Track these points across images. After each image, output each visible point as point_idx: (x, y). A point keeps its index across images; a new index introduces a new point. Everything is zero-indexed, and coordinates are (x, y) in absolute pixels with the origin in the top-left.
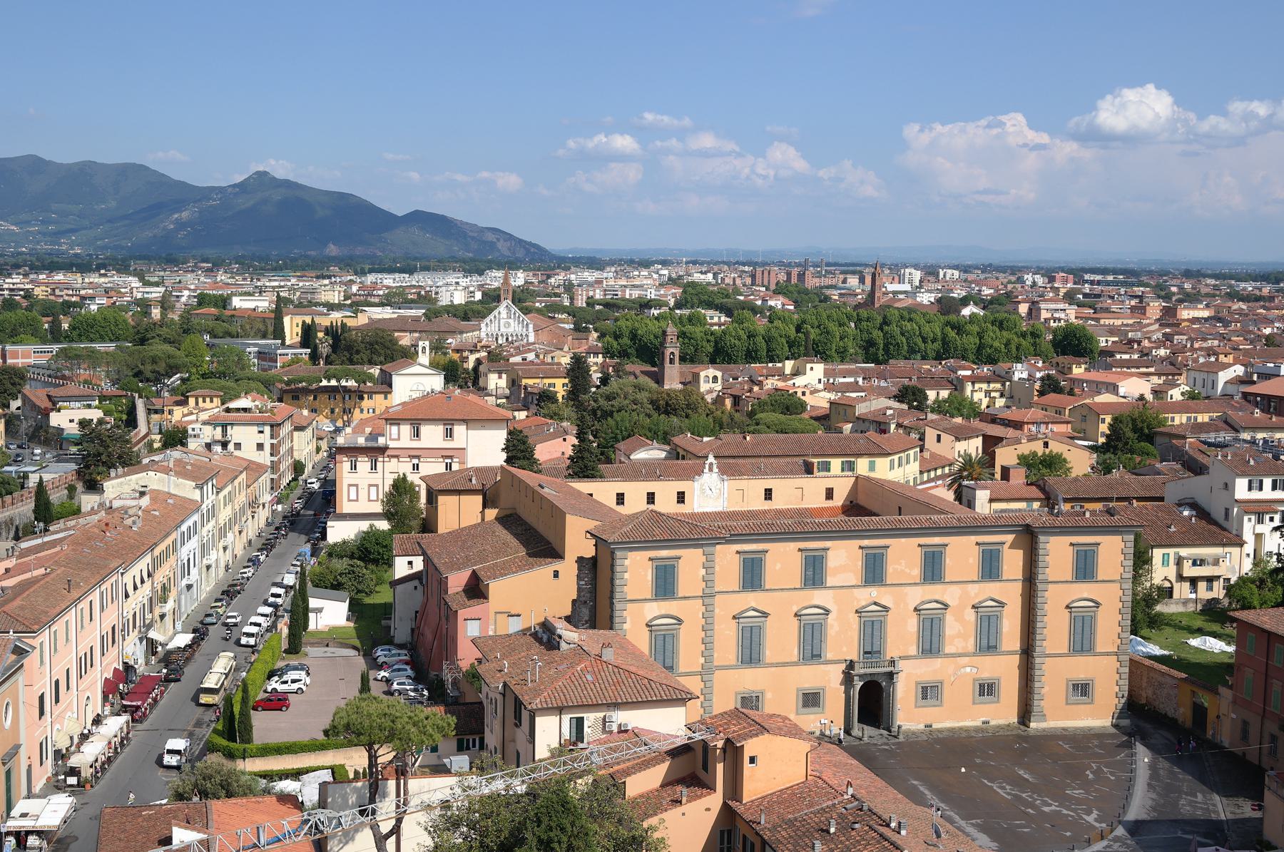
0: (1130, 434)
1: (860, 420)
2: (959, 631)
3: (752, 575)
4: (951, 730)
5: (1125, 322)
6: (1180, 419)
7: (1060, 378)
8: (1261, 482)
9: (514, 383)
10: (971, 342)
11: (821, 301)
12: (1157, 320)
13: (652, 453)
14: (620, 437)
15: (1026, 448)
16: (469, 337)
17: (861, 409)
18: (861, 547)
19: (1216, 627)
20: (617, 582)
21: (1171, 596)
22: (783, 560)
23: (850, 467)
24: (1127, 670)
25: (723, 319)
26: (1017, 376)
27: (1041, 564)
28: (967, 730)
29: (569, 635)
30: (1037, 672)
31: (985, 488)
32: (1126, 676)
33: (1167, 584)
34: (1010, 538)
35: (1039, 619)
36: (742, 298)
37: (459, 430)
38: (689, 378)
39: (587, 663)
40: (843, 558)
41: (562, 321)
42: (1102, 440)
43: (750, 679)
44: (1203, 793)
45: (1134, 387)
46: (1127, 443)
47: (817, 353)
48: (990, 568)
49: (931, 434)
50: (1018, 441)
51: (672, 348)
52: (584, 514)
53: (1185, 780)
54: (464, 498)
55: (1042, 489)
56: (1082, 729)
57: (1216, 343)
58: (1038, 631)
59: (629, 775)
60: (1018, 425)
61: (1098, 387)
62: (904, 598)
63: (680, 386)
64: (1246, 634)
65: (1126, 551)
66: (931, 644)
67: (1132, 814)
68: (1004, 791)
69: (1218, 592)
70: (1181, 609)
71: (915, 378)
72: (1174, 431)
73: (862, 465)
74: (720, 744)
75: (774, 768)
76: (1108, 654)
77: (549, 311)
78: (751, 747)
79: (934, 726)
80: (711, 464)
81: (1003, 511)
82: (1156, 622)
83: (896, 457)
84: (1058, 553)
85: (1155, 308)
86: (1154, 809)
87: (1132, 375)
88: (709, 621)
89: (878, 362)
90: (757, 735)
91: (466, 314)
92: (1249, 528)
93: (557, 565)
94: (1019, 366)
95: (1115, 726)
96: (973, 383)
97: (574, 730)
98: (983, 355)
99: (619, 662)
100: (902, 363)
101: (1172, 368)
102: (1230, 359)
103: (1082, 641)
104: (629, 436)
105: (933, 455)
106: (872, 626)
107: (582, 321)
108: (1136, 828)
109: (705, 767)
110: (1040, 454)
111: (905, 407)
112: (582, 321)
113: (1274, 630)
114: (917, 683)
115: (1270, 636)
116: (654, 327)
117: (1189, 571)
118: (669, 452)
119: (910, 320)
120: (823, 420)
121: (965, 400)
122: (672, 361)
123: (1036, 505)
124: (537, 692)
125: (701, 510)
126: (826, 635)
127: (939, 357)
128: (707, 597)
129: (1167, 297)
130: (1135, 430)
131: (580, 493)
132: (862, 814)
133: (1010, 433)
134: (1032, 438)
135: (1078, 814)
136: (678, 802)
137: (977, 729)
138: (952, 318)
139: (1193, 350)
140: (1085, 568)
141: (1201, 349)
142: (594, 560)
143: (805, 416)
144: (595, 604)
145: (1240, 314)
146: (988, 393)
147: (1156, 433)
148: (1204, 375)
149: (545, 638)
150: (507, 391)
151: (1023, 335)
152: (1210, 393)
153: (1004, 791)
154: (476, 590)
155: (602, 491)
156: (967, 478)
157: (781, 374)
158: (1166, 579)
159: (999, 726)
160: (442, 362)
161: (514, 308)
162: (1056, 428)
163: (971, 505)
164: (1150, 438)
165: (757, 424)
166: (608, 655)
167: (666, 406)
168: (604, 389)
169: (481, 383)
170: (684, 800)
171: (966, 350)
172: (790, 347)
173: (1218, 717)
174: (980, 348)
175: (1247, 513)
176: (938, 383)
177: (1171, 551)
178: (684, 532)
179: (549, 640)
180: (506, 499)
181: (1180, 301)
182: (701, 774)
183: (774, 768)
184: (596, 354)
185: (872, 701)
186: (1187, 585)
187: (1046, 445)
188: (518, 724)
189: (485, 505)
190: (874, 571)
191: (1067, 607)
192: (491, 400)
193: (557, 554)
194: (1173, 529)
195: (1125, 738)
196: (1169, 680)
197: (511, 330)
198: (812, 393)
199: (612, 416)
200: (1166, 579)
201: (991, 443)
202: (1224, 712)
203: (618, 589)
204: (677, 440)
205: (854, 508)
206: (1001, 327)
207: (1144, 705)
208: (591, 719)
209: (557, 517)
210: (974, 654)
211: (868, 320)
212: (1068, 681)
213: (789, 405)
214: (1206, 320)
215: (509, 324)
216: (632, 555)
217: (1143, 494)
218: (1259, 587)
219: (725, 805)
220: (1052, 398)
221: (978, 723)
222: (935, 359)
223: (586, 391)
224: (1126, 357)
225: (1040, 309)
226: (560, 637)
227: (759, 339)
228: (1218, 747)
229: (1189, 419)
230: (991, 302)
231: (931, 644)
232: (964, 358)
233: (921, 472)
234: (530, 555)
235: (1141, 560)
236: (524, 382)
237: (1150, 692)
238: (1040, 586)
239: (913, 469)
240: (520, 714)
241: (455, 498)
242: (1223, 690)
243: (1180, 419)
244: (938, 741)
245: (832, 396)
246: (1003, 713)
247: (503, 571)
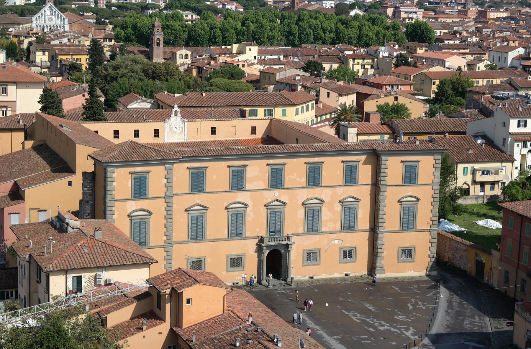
0: (450, 92)
1: (279, 82)
2: (331, 218)
3: (198, 183)
4: (326, 280)
5: (454, 20)
6: (482, 82)
7: (408, 55)
8: (526, 121)
9: (53, 58)
10: (354, 32)
11: (261, 6)
12: (474, 19)
13: (141, 104)
14: (122, 94)
15: (382, 101)
16: (24, 27)
17: (280, 76)
18: (268, 165)
19: (495, 213)
20: (108, 188)
21: (468, 194)
22: (218, 173)
23: (270, 113)
24: (436, 240)
25: (195, 16)
26: (382, 54)
27: (382, 174)
28: (335, 279)
29: (74, 223)
30: (380, 243)
31: (354, 126)
32: (435, 244)
33: (466, 187)
34: (363, 158)
35: (381, 209)
36: (209, 3)
37: (11, 89)
38: (170, 56)
39: (85, 241)
40: (257, 171)
41: (89, 17)
42: (433, 96)
43: (196, 250)
44: (479, 316)
45: (455, 62)
46: (448, 98)
47: (254, 39)
48: (351, 177)
49: (323, 92)
50: (379, 97)
51: (158, 36)
52: (88, 144)
53: (469, 308)
54: (14, 134)
55: (390, 127)
56: (404, 278)
57: (509, 33)
58: (381, 217)
59: (109, 312)
60: (379, 86)
61: (432, 62)
62: (295, 197)
63: (164, 61)
64: (509, 218)
65: (436, 165)
66: (313, 225)
67: (435, 329)
68: (356, 317)
69: (498, 191)
70: (474, 202)
71: (316, 56)
72: (478, 90)
73: (278, 113)
74: (168, 291)
75: (202, 306)
76: (424, 231)
77: (80, 11)
78: (187, 293)
79: (315, 278)
80: (176, 112)
81: (365, 141)
82: (458, 210)
83: (299, 107)
84: (394, 167)
85: (473, 11)
86: (448, 326)
87: (454, 54)
88: (169, 212)
89: (294, 45)
90: (191, 285)
91: (22, 12)
92: (518, 151)
93: (71, 178)
94: (383, 48)
95: (428, 276)
96: (354, 59)
97: (75, 284)
98: (362, 41)
99: (106, 240)
100: (309, 46)
101: (480, 50)
102: (516, 44)
103: (408, 223)
104: (128, 93)
105: (324, 105)
106: (275, 215)
107: (101, 17)
108: (436, 339)
109: (159, 307)
110: (391, 105)
111: (308, 74)
112: (101, 17)
113: (525, 214)
114: (304, 251)
115: (523, 218)
116: (148, 22)
117: (480, 178)
118: (152, 104)
119: (316, 18)
120: (256, 83)
121: (348, 70)
122: (158, 44)
123: (386, 137)
124: (50, 260)
125: (170, 141)
126: (245, 221)
127: (333, 43)
128: (168, 197)
129: (482, 5)
130: (453, 89)
131: (88, 130)
132: (259, 335)
133: (375, 91)
134: (387, 95)
135: (401, 331)
136: (140, 329)
137: (341, 279)
138: (343, 17)
139: (494, 38)
140: (410, 176)
141: (499, 37)
142: (93, 174)
143: (244, 80)
144: (94, 202)
145: (526, 15)
146: (363, 66)
147: (467, 91)
148: (499, 54)
149: (58, 225)
150: (49, 64)
151: (388, 28)
152: (503, 65)
153: (356, 317)
154: (16, 195)
155: (105, 129)
156: (343, 120)
157: (230, 53)
158: (465, 183)
159: (356, 278)
160: (5, 44)
161: (54, 8)
162: (403, 88)
163: (345, 137)
164: (463, 95)
165: (212, 85)
166: (99, 235)
167: (153, 74)
168: (114, 63)
169: (31, 58)
170: (145, 328)
171: (351, 38)
172: (237, 35)
173: (491, 269)
174: (360, 36)
175: (516, 141)
176: (331, 59)
177: (469, 166)
178: (153, 155)
179: (61, 226)
180: (39, 135)
181: (490, 7)
182: (157, 311)
183: (202, 306)
184: (110, 39)
185: (275, 261)
186: (478, 187)
187: (396, 99)
188: (39, 282)
189: (26, 139)
190: (276, 180)
191: (399, 201)
192: (37, 69)
193: (69, 169)
194: (470, 152)
195: (433, 283)
196: (462, 246)
197: (53, 23)
198: (249, 65)
199: (116, 81)
200: (465, 183)
201: (362, 97)
202: (495, 267)
203: (109, 193)
204: (158, 96)
205: (269, 139)
206: (374, 23)
207: (446, 263)
208: (87, 277)
209: (71, 146)
210: (340, 232)
211: (289, 18)
212: (399, 248)
213: (233, 73)
214: (504, 19)
215: (52, 19)
216: (118, 170)
217: (453, 130)
218: (522, 188)
219: (171, 330)
220: (403, 69)
221: (342, 275)
222: (331, 44)
223: (101, 63)
224: (451, 42)
225: (400, 12)
226: (67, 224)
227: (217, 30)
228: (488, 287)
229: (488, 82)
230: (370, 7)
231: (313, 225)
232: (349, 43)
233: (316, 117)
234: (53, 171)
235: (447, 171)
236: (60, 57)
237: (450, 255)
238: (382, 188)
239: (311, 114)
240: (40, 276)
241: (8, 134)
242: (494, 252)
243: (482, 82)
244: (317, 287)
245: (261, 68)
246: (358, 269)
247: (34, 182)
